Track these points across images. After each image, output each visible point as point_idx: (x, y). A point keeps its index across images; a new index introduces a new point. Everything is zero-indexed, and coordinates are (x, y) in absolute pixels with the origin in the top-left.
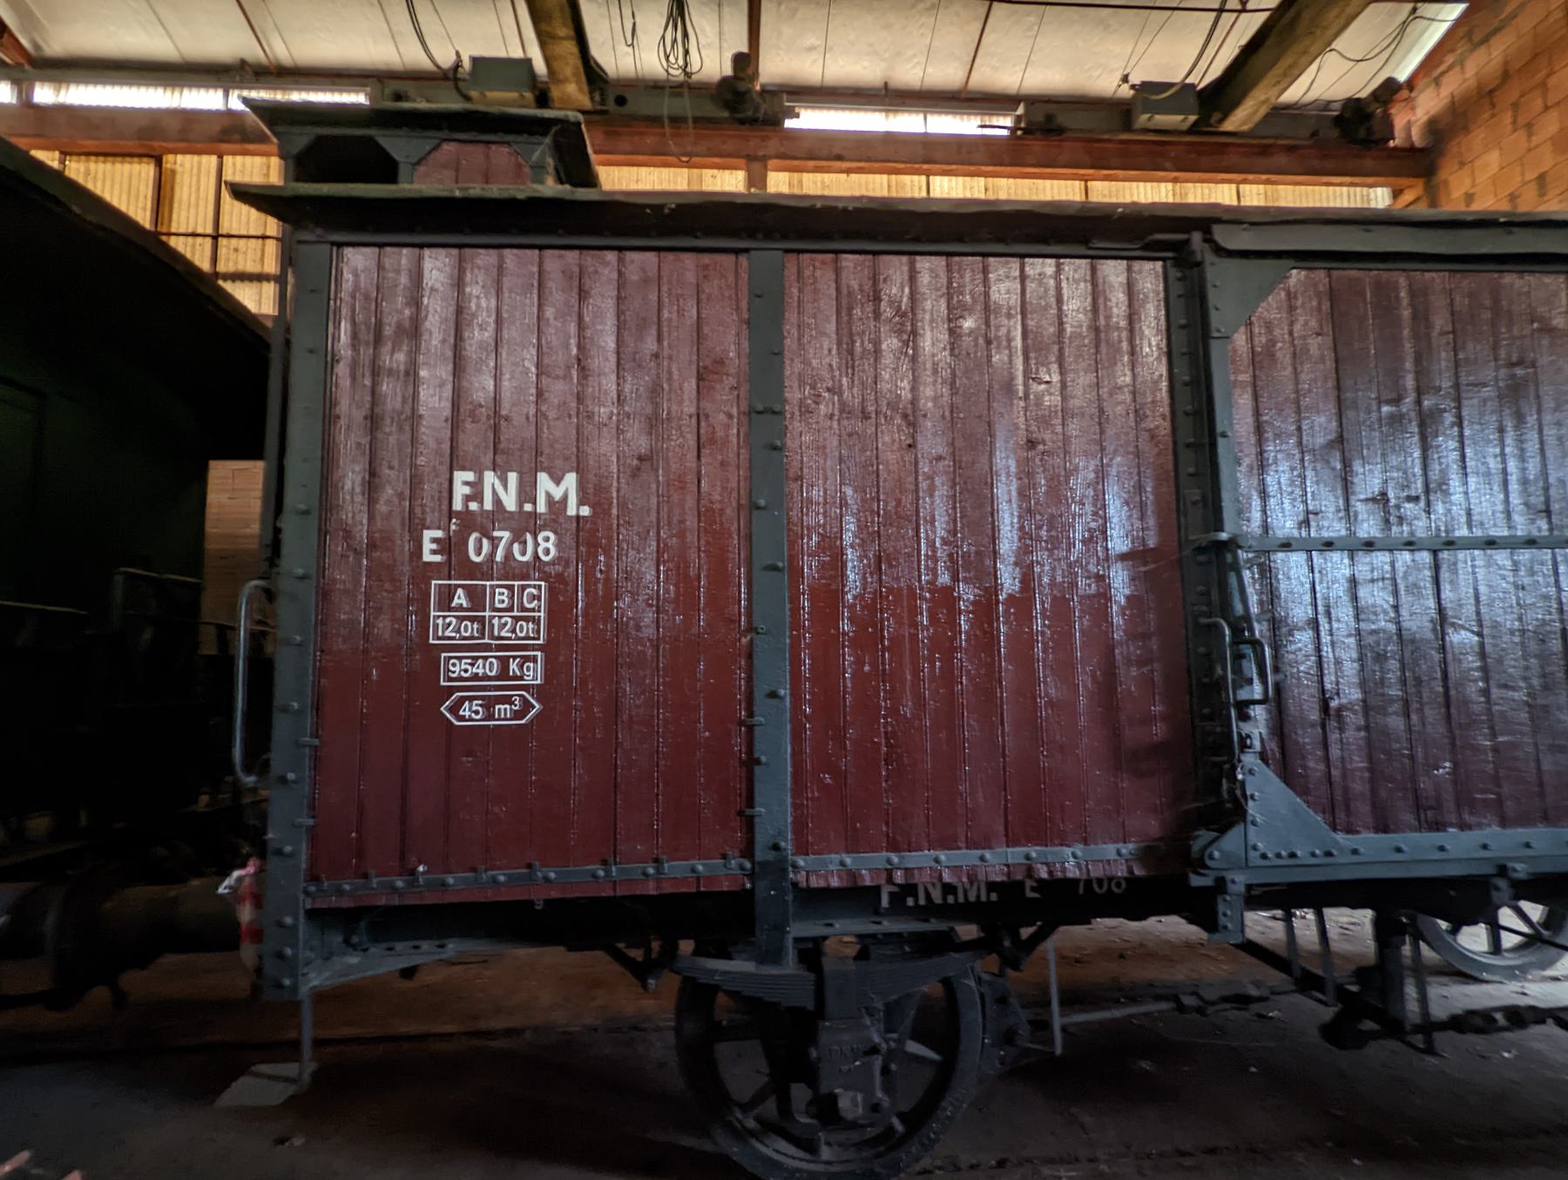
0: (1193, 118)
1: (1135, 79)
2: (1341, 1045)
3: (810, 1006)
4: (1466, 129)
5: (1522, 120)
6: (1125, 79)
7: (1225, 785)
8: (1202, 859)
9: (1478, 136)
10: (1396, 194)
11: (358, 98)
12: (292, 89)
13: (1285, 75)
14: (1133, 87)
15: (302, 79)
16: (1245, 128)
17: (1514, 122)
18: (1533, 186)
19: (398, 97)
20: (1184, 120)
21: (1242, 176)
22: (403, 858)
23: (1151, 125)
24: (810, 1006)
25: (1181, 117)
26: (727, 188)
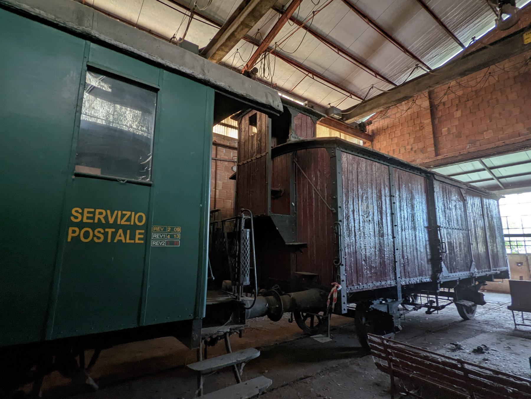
0: (341, 117)
1: (332, 105)
2: (428, 314)
3: (387, 312)
4: (379, 134)
5: (391, 137)
6: (329, 104)
7: (440, 265)
8: (439, 278)
9: (382, 137)
10: (364, 143)
11: (302, 104)
12: (297, 100)
13: (362, 117)
14: (331, 106)
15: (104, 11)
16: (349, 123)
17: (389, 137)
18: (392, 151)
19: (312, 107)
20: (339, 117)
21: (341, 131)
22: (358, 282)
23: (333, 117)
24: (387, 312)
25: (338, 117)
26: (354, 142)
